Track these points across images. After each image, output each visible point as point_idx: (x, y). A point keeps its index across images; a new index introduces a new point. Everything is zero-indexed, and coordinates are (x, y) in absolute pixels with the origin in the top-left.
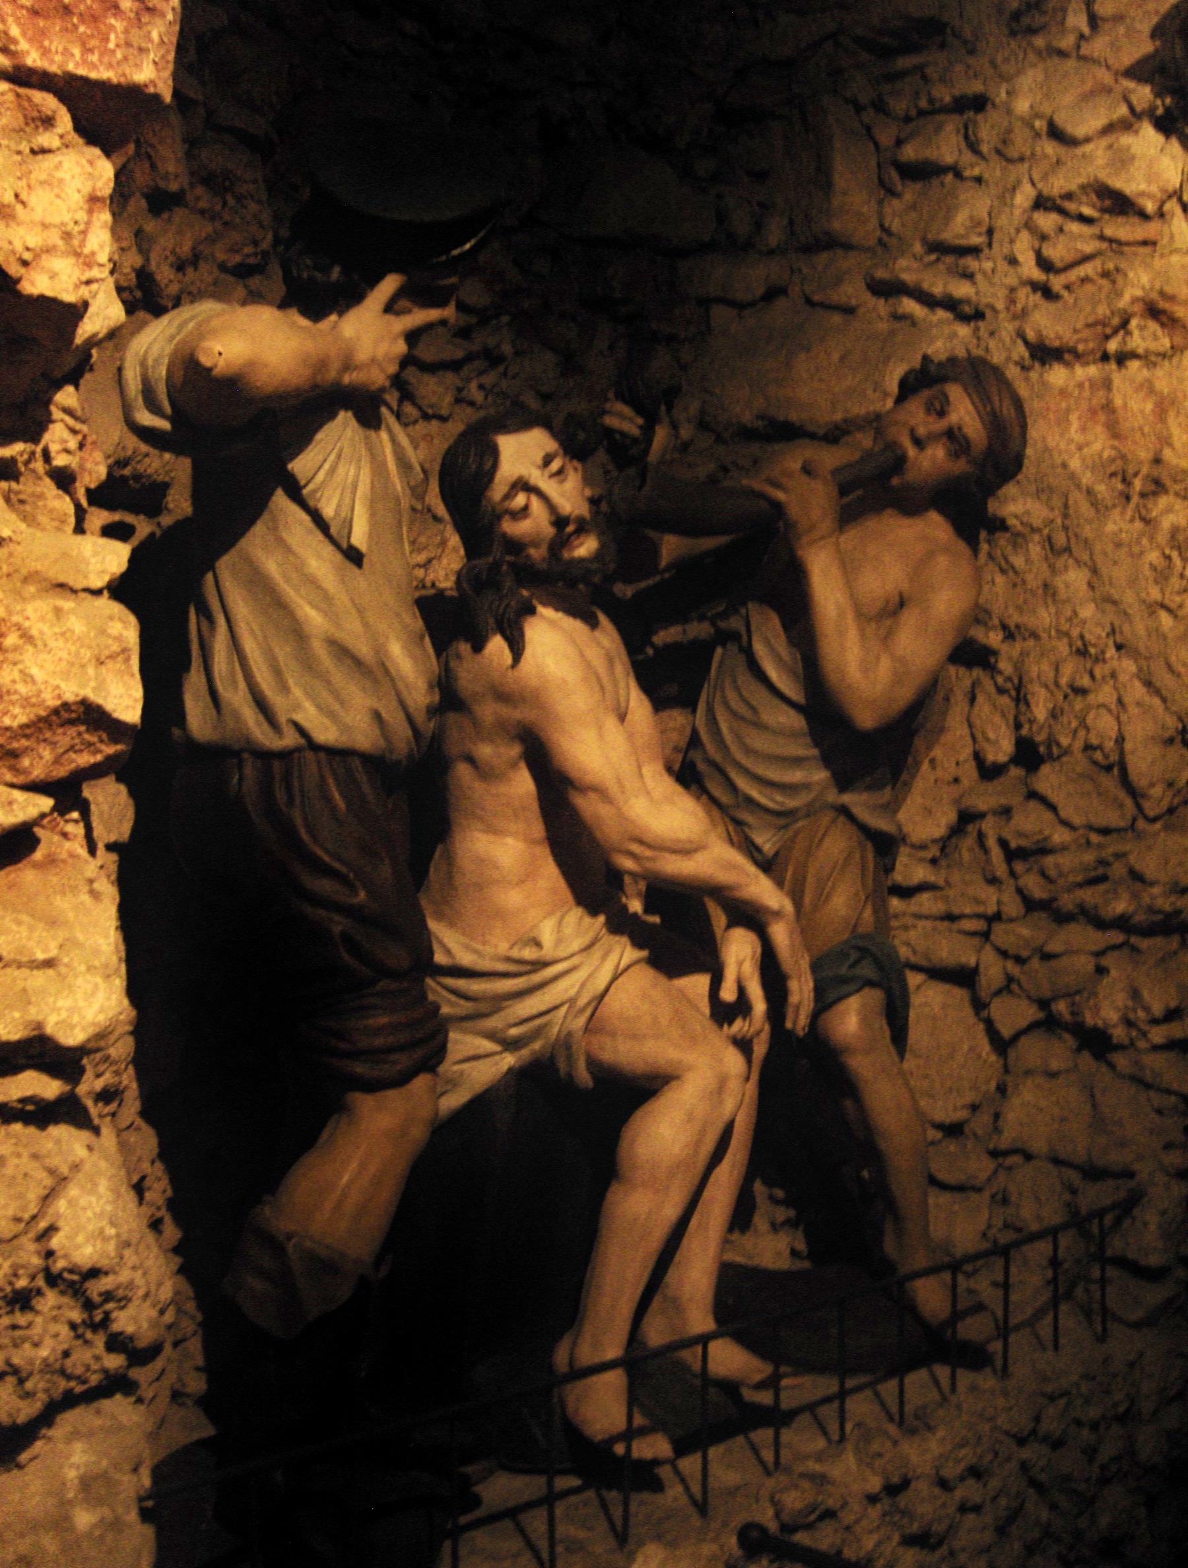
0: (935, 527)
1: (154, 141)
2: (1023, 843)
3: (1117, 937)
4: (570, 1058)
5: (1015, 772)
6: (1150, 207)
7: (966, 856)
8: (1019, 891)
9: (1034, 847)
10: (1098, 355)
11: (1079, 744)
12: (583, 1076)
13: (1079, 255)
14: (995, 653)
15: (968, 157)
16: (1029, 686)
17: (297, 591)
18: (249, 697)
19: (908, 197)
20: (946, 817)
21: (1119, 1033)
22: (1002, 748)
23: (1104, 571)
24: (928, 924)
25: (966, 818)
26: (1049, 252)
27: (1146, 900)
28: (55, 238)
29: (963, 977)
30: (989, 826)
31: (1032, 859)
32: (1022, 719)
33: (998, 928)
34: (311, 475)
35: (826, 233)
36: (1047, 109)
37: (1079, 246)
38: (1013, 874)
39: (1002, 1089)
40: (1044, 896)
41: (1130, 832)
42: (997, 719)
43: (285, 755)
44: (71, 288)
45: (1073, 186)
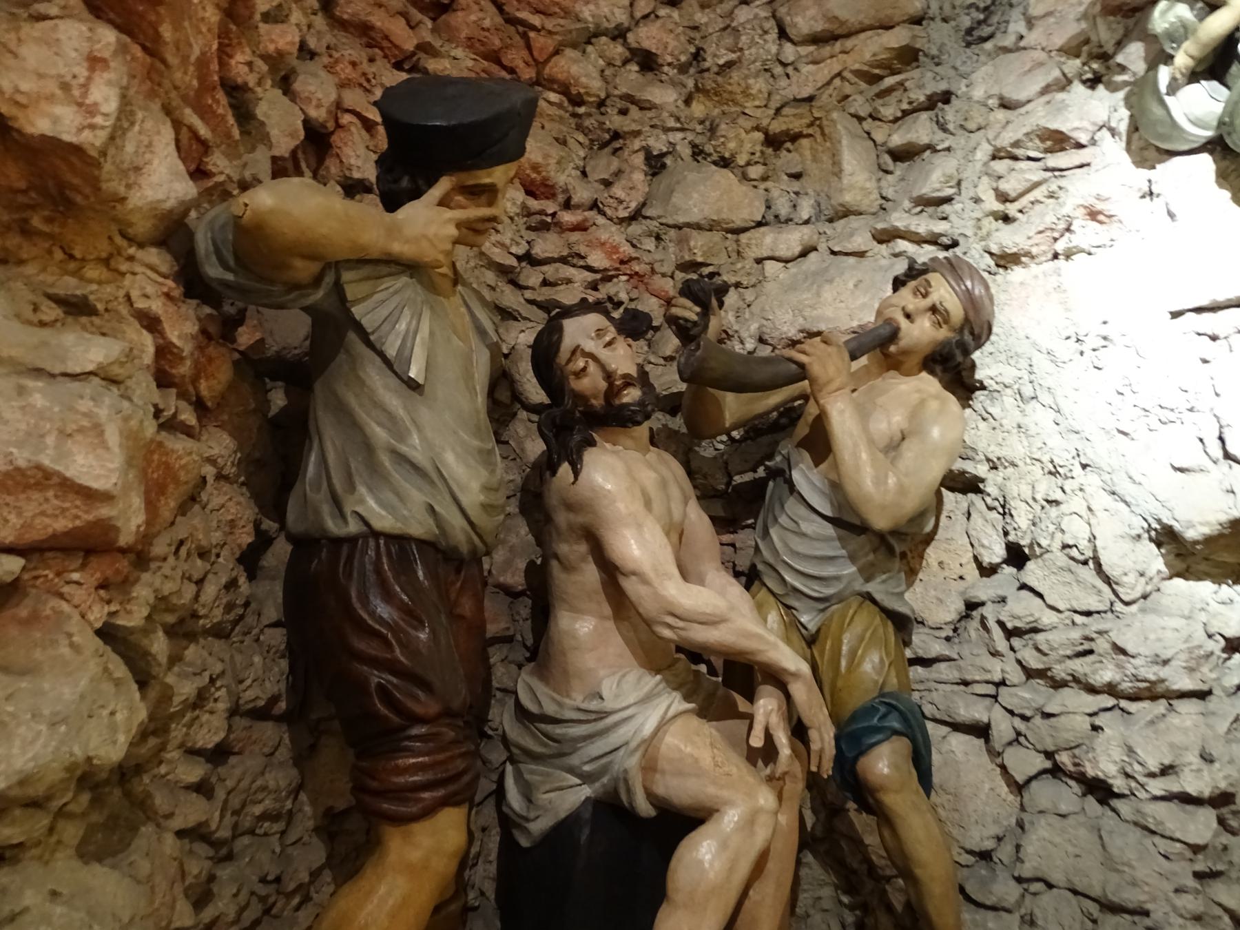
0: (928, 383)
1: (340, 144)
2: (1019, 624)
3: (1109, 701)
4: (629, 791)
5: (1008, 570)
6: (1083, 139)
7: (973, 634)
8: (1019, 662)
9: (1028, 627)
10: (1050, 256)
11: (1057, 545)
12: (644, 808)
13: (1028, 185)
14: (983, 481)
15: (941, 135)
16: (1012, 503)
17: (368, 415)
18: (329, 496)
19: (898, 173)
20: (955, 606)
21: (1119, 784)
22: (995, 552)
23: (1065, 409)
24: (948, 688)
25: (971, 606)
26: (1004, 186)
27: (1130, 670)
28: (52, 87)
29: (981, 731)
30: (989, 611)
31: (1026, 637)
32: (1009, 528)
33: (1003, 690)
34: (377, 325)
35: (842, 205)
36: (995, 90)
37: (1028, 176)
38: (1012, 649)
39: (1020, 825)
40: (1040, 666)
41: (1109, 614)
42: (990, 530)
43: (352, 540)
44: (74, 130)
45: (1019, 135)
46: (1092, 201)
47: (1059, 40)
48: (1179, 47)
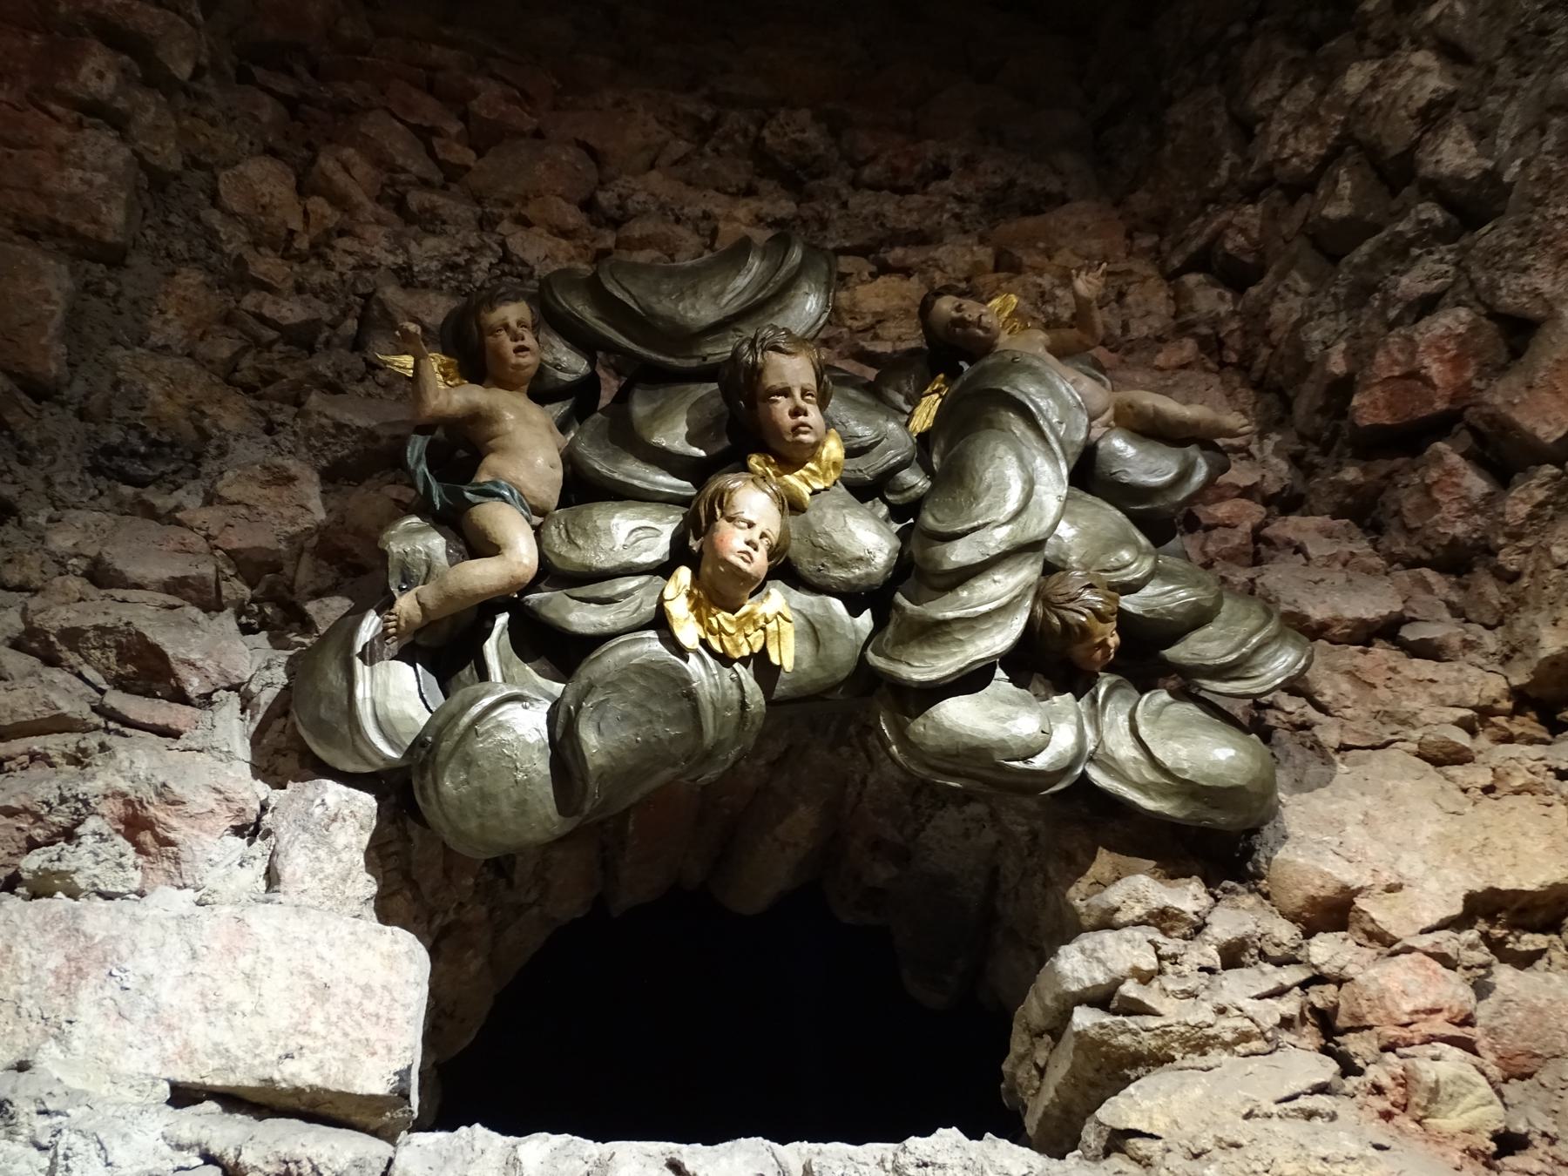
6: (194, 686)
46: (147, 793)
47: (237, 539)
48: (408, 590)
